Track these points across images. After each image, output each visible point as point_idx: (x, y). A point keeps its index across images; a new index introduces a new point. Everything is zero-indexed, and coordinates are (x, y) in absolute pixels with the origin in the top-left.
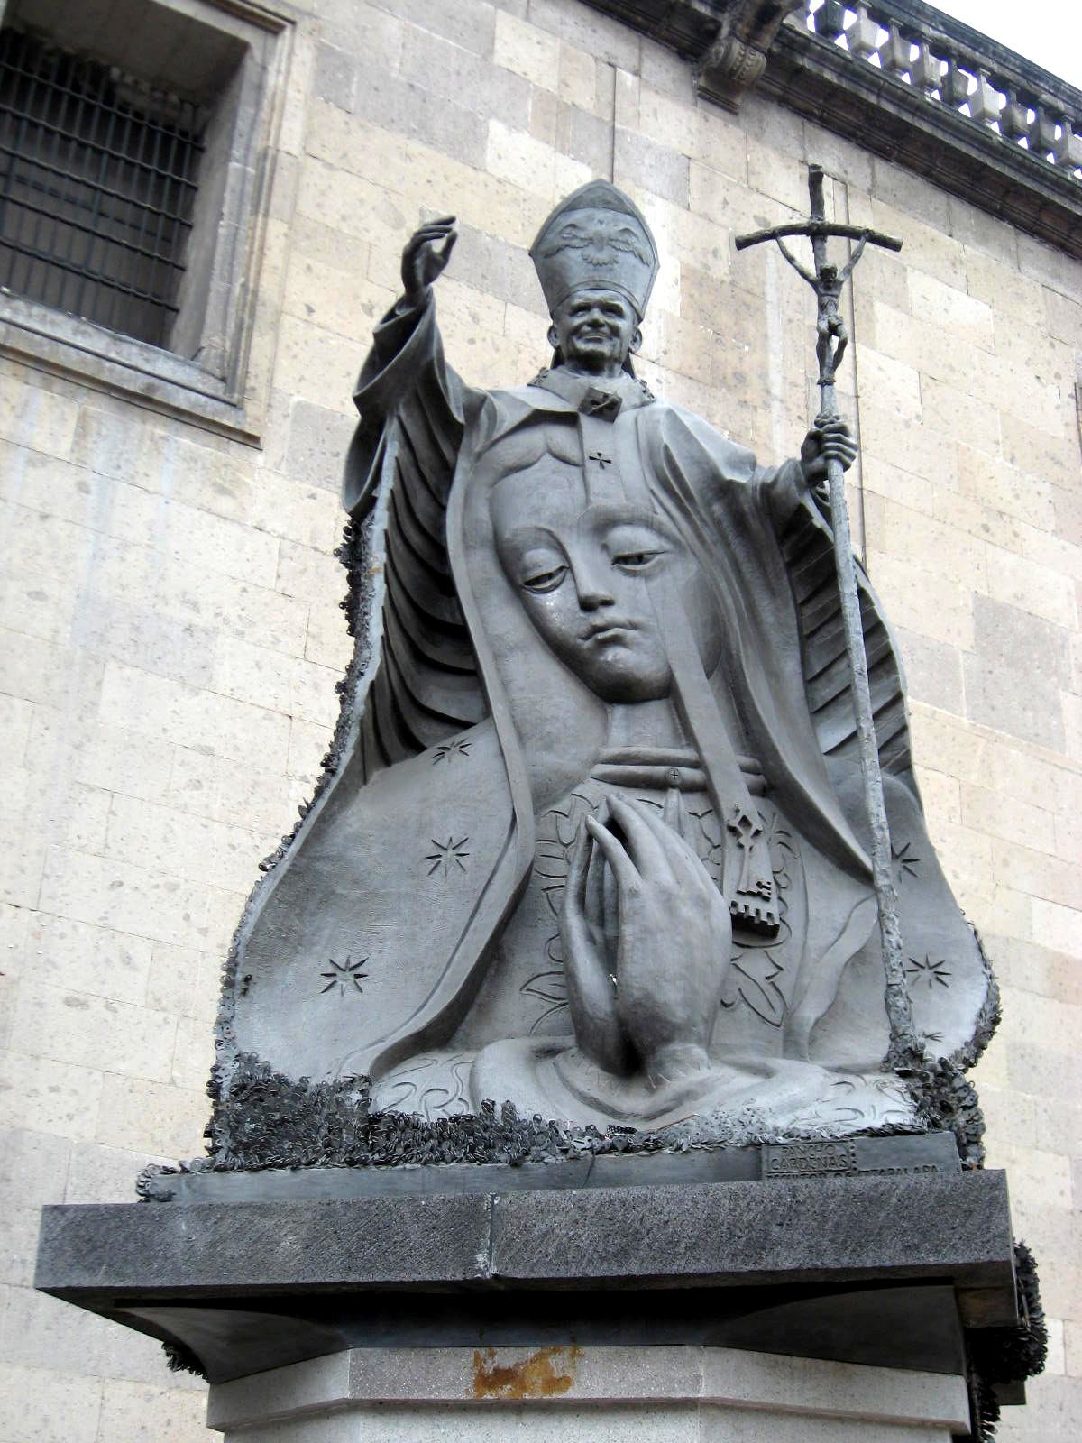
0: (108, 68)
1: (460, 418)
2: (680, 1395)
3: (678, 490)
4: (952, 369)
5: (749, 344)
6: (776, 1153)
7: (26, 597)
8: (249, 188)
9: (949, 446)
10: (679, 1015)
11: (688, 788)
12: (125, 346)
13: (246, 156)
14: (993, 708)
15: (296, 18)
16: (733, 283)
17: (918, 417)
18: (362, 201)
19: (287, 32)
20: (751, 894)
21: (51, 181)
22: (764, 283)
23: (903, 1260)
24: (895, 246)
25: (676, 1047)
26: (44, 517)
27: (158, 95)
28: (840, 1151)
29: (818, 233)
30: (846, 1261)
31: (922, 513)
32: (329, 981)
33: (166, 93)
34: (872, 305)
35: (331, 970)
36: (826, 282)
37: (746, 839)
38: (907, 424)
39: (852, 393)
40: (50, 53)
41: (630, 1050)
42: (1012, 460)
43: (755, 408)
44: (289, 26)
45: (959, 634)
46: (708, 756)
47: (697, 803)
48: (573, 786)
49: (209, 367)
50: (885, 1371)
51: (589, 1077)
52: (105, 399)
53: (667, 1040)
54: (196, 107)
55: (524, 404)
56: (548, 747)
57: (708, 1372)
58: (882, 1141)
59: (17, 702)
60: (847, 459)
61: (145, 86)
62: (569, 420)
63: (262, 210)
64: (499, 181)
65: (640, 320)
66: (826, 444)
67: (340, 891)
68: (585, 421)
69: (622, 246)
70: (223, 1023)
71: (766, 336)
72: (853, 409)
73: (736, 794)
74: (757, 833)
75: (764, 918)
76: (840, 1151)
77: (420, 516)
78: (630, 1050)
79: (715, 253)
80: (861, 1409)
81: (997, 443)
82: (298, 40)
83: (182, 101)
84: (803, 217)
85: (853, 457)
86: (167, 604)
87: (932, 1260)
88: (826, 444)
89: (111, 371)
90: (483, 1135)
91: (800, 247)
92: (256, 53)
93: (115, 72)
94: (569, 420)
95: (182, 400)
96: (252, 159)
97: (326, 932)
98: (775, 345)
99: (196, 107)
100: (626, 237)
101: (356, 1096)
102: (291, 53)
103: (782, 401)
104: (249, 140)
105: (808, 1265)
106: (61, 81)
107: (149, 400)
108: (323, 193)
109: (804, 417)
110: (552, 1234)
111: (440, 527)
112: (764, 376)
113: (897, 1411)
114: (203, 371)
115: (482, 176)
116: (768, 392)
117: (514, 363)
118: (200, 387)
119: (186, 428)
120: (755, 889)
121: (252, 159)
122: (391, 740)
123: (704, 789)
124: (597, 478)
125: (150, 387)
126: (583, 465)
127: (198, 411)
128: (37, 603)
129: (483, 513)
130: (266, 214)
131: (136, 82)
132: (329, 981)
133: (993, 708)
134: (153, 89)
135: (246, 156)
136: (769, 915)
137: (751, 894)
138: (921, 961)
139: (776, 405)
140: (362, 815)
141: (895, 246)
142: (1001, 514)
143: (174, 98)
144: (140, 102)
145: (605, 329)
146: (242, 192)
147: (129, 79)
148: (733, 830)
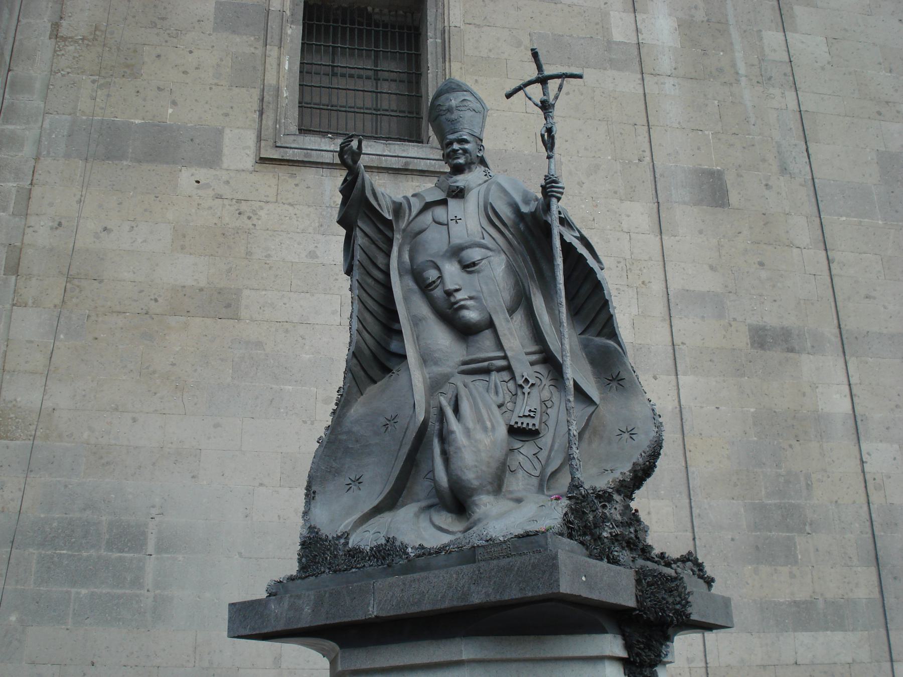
1: (389, 217)
2: (455, 659)
4: (846, 30)
5: (723, 51)
6: (480, 550)
8: (439, 50)
9: (850, 73)
10: (476, 483)
11: (500, 370)
12: (392, 146)
13: (435, 34)
14: (897, 212)
16: (708, 21)
17: (829, 63)
18: (498, 39)
20: (524, 416)
21: (349, 71)
22: (727, 15)
23: (519, 596)
24: (580, 77)
25: (476, 498)
28: (504, 546)
29: (543, 80)
30: (498, 597)
31: (839, 115)
32: (348, 487)
34: (792, 9)
35: (350, 482)
36: (546, 107)
37: (527, 389)
38: (823, 68)
39: (788, 60)
41: (457, 502)
42: (890, 71)
43: (731, 84)
45: (871, 175)
46: (509, 354)
47: (505, 375)
48: (448, 379)
49: (434, 145)
50: (563, 636)
51: (445, 519)
52: (386, 175)
53: (471, 496)
54: (412, 14)
56: (436, 363)
57: (466, 649)
58: (524, 539)
60: (561, 190)
61: (386, 11)
62: (444, 202)
63: (447, 60)
64: (569, 6)
65: (481, 140)
66: (550, 189)
67: (350, 446)
68: (449, 200)
69: (463, 108)
70: (305, 513)
71: (731, 44)
72: (790, 69)
73: (524, 368)
74: (533, 385)
75: (530, 427)
76: (504, 546)
77: (380, 266)
78: (457, 502)
79: (696, 8)
80: (552, 655)
81: (880, 64)
83: (405, 13)
84: (533, 73)
85: (562, 193)
87: (530, 594)
88: (550, 189)
89: (386, 161)
90: (388, 555)
91: (536, 91)
93: (370, 9)
94: (444, 202)
95: (422, 165)
97: (347, 466)
98: (738, 46)
99: (412, 14)
100: (465, 103)
101: (342, 541)
103: (746, 76)
104: (435, 26)
105: (485, 600)
106: (344, 22)
108: (477, 41)
109: (760, 81)
110: (434, 591)
111: (388, 265)
112: (734, 65)
113: (571, 654)
114: (432, 148)
115: (559, 6)
116: (737, 73)
117: (592, 98)
118: (432, 157)
119: (427, 178)
120: (527, 413)
121: (439, 35)
122: (375, 372)
123: (509, 368)
124: (455, 228)
125: (406, 164)
126: (447, 225)
127: (432, 169)
129: (406, 257)
130: (450, 61)
132: (348, 487)
133: (897, 212)
134: (390, 12)
135: (435, 34)
136: (534, 425)
137: (524, 416)
138: (624, 429)
139: (743, 79)
140: (357, 410)
141: (580, 77)
142: (887, 103)
145: (460, 151)
147: (377, 10)
148: (521, 387)
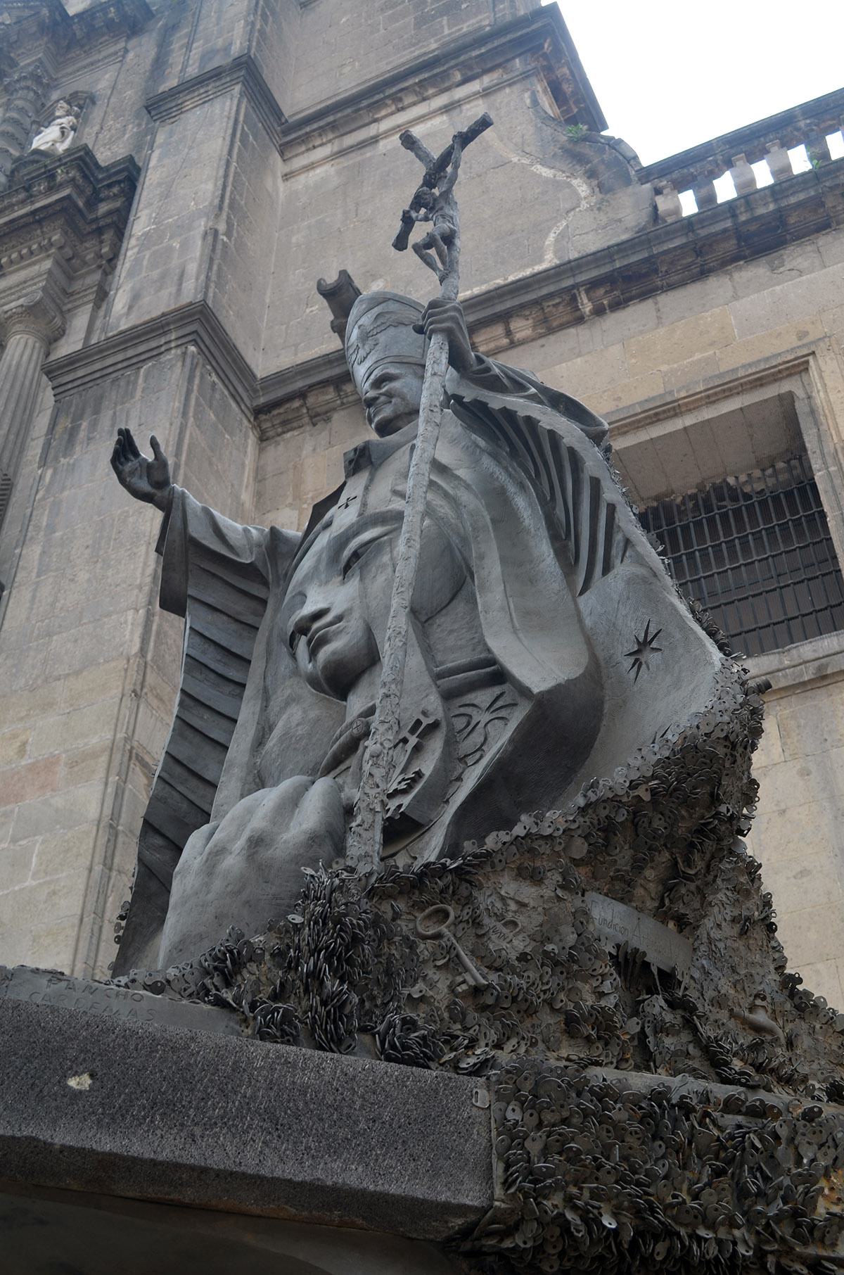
0: (725, 480)
3: (9, 414)
7: (793, 880)
13: (825, 463)
15: (813, 348)
19: (812, 362)
26: (783, 812)
27: (770, 471)
33: (773, 466)
40: (683, 502)
44: (811, 359)
55: (251, 653)
59: (819, 966)
61: (757, 473)
82: (820, 361)
83: (788, 462)
86: (829, 893)
92: (800, 393)
93: (731, 481)
96: (829, 460)
102: (820, 372)
107: (824, 677)
125: (819, 669)
128: (804, 880)
131: (749, 475)
134: (763, 470)
135: (825, 463)
143: (780, 465)
144: (759, 486)
146: (833, 487)
